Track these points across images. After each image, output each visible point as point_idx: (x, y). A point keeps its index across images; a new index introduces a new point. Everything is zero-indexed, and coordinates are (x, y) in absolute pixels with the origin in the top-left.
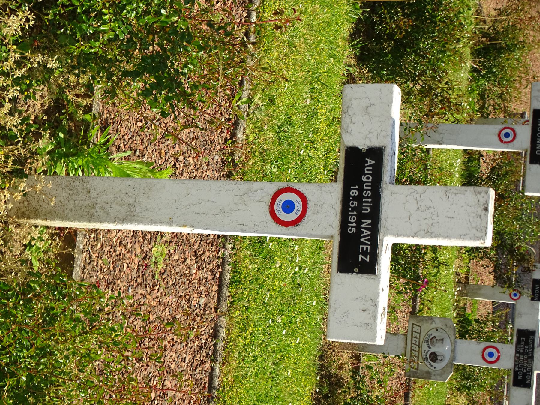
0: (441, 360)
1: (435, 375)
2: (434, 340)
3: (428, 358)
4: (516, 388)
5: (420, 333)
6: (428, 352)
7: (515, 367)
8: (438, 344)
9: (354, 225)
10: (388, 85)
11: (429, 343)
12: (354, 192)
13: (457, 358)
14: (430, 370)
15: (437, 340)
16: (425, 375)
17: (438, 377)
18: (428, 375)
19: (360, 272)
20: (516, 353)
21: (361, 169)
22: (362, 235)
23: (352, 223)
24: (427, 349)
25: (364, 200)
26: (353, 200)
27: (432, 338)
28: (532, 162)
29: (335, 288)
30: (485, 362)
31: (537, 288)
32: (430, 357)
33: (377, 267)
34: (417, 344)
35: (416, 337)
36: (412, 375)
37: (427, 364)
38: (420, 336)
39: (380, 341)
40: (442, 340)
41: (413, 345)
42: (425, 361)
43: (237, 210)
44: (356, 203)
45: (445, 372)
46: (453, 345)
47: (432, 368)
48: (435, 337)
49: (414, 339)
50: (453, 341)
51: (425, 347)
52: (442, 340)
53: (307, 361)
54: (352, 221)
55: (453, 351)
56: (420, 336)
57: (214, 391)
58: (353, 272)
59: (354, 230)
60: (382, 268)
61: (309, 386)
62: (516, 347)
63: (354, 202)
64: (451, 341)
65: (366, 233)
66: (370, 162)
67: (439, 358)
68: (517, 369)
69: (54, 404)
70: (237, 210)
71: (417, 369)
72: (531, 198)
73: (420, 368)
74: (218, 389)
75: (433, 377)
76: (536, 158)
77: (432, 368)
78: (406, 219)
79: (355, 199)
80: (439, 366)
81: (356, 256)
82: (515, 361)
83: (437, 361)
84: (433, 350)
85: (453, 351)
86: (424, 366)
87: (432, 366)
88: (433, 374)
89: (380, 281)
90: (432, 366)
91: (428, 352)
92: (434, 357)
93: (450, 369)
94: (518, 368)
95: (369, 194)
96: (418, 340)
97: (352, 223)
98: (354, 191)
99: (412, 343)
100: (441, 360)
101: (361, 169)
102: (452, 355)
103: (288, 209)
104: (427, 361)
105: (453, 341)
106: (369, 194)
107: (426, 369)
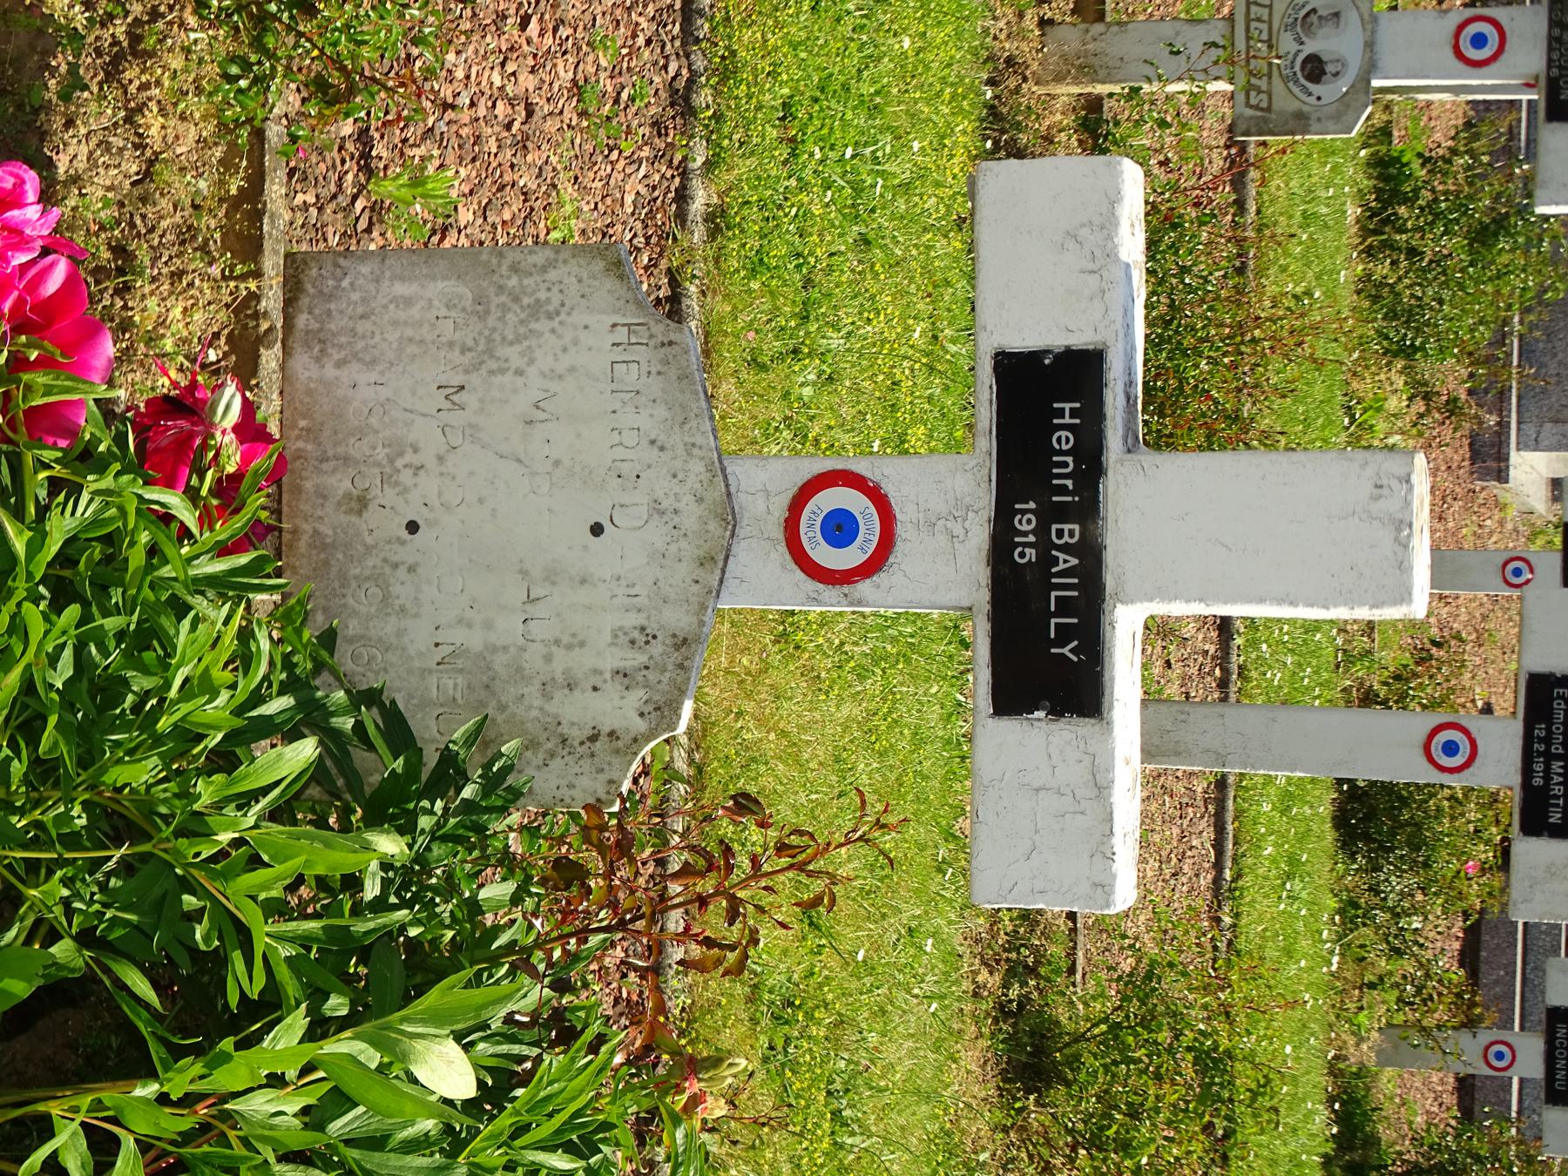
0: (1336, 74)
1: (1319, 120)
2: (1314, 18)
3: (1299, 74)
4: (1555, 125)
5: (1270, 7)
6: (1296, 55)
7: (1549, 67)
8: (1326, 30)
9: (1031, 538)
11: (1299, 29)
13: (1380, 64)
14: (1306, 109)
15: (1320, 17)
16: (1292, 124)
17: (1330, 125)
18: (1300, 122)
20: (1550, 27)
21: (1044, 413)
23: (1025, 534)
24: (1295, 47)
27: (1307, 15)
29: (982, 740)
30: (1435, 772)
31: (1561, 1033)
32: (1303, 69)
34: (1265, 36)
35: (1259, 20)
36: (1253, 130)
37: (1296, 90)
38: (1270, 14)
40: (1337, 15)
41: (1252, 43)
42: (1291, 84)
44: (1542, 748)
45: (1348, 106)
46: (1369, 27)
47: (1312, 100)
48: (1314, 11)
49: (1253, 25)
50: (1366, 16)
51: (1287, 43)
52: (1337, 15)
54: (1025, 527)
55: (1370, 45)
56: (1270, 14)
57: (699, 22)
59: (1031, 553)
62: (1551, 10)
64: (1361, 17)
65: (1066, 561)
67: (1330, 68)
68: (1555, 72)
71: (1269, 109)
72: (1546, 218)
73: (1275, 106)
74: (713, 17)
75: (1315, 126)
76: (1560, 110)
77: (1312, 100)
78: (1179, 541)
79: (1541, 740)
80: (1331, 91)
82: (1550, 49)
83: (1324, 78)
84: (1310, 47)
85: (1370, 45)
86: (1285, 99)
87: (1310, 94)
88: (1314, 117)
90: (1310, 94)
91: (1296, 55)
92: (1315, 69)
93: (1363, 98)
94: (1560, 67)
96: (1264, 27)
97: (1025, 534)
99: (1248, 38)
100: (1336, 74)
101: (1044, 413)
102: (1368, 55)
104: (1296, 82)
105: (1366, 16)
107: (1294, 105)
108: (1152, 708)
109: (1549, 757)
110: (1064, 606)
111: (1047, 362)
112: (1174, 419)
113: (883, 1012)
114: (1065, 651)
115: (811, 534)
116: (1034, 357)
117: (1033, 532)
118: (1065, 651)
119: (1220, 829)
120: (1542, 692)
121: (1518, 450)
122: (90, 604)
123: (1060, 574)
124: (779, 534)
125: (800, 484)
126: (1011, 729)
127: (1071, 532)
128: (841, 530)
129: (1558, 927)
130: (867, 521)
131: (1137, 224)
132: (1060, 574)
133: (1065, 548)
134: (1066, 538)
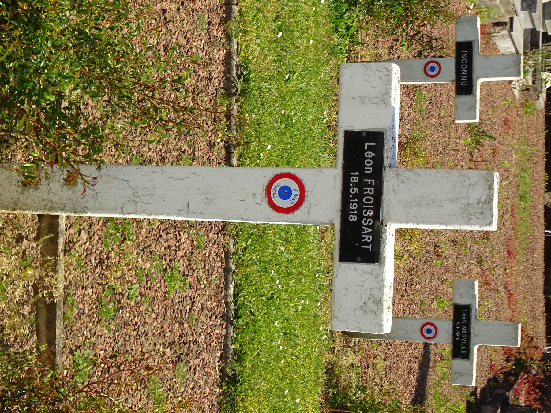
9: (356, 212)
10: (387, 64)
12: (355, 179)
21: (362, 154)
22: (363, 233)
23: (353, 210)
26: (353, 187)
33: (376, 130)
39: (387, 328)
43: (233, 195)
44: (356, 190)
54: (354, 208)
63: (355, 189)
66: (370, 154)
69: (296, 2)
70: (233, 195)
78: (414, 205)
97: (353, 210)
101: (362, 154)
103: (286, 194)
108: (395, 319)
109: (461, 325)
110: (464, 346)
111: (359, 258)
113: (259, 342)
115: (274, 192)
116: (359, 134)
119: (422, 380)
123: (365, 234)
124: (420, 331)
126: (345, 265)
128: (286, 194)
130: (295, 193)
132: (365, 234)
133: (368, 226)
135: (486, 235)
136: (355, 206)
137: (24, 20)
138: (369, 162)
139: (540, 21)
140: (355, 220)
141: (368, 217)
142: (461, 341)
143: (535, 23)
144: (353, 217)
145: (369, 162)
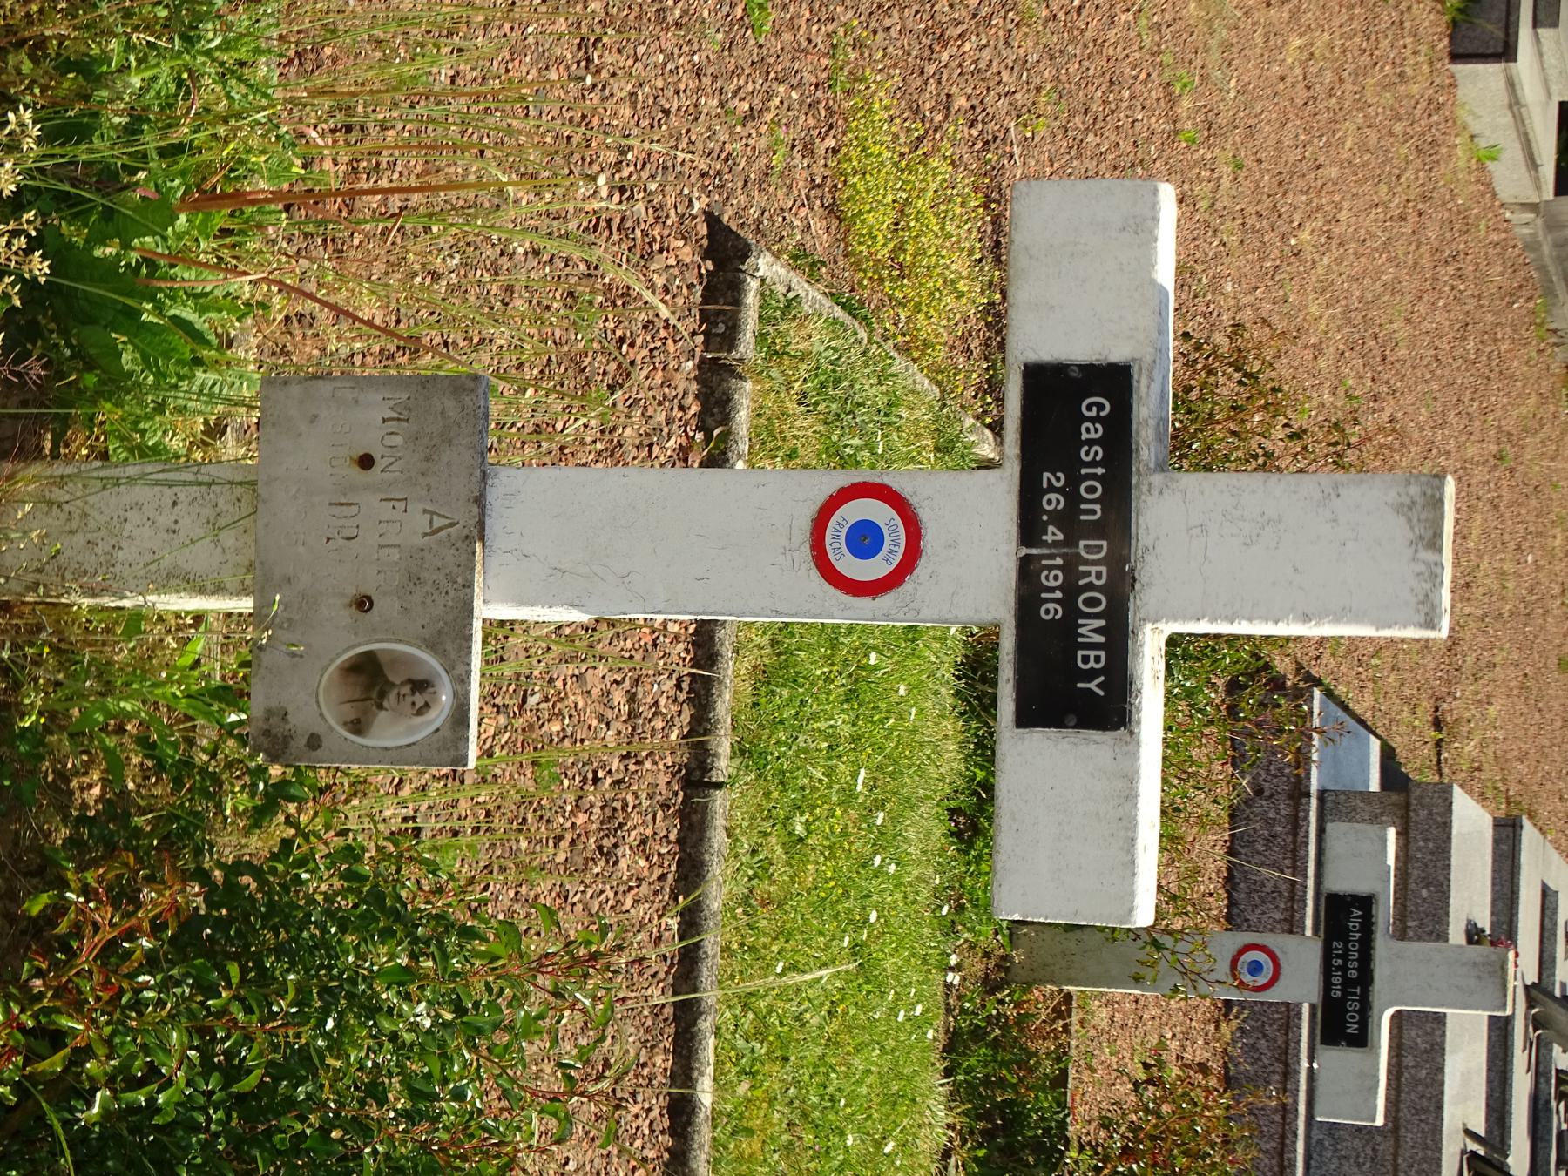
9: (1058, 594)
19: (1349, 1045)
21: (1072, 429)
25: (1083, 471)
28: (1026, 718)
39: (1380, 1121)
53: (917, 1001)
54: (1053, 583)
58: (1081, 367)
60: (1145, 705)
61: (936, 1117)
78: (1212, 563)
79: (1338, 956)
81: (1061, 672)
89: (1138, 744)
95: (1096, 453)
98: (1051, 606)
101: (1072, 429)
103: (865, 538)
106: (1096, 453)
112: (1189, 451)
114: (1092, 686)
117: (1060, 588)
118: (1092, 686)
120: (1562, 104)
121: (1490, 1017)
122: (75, 1050)
125: (819, 504)
127: (1094, 551)
129: (1490, 1017)
130: (895, 542)
131: (1158, 658)
134: (1092, 664)
135: (1426, 645)
136: (1047, 611)
137: (202, 221)
138: (1091, 490)
139: (1532, 163)
140: (1060, 507)
141: (1091, 443)
142: (1072, 615)
143: (1519, 156)
144: (1092, 654)
145: (1091, 490)
